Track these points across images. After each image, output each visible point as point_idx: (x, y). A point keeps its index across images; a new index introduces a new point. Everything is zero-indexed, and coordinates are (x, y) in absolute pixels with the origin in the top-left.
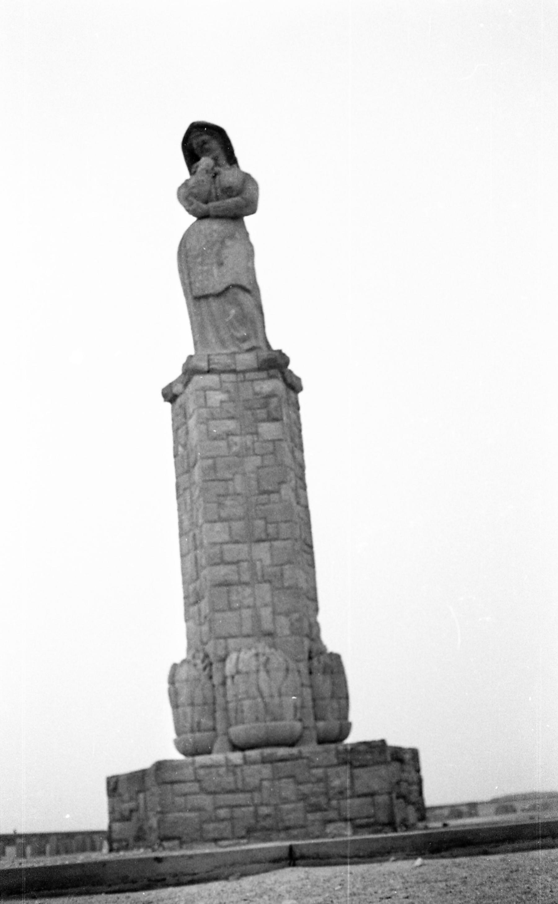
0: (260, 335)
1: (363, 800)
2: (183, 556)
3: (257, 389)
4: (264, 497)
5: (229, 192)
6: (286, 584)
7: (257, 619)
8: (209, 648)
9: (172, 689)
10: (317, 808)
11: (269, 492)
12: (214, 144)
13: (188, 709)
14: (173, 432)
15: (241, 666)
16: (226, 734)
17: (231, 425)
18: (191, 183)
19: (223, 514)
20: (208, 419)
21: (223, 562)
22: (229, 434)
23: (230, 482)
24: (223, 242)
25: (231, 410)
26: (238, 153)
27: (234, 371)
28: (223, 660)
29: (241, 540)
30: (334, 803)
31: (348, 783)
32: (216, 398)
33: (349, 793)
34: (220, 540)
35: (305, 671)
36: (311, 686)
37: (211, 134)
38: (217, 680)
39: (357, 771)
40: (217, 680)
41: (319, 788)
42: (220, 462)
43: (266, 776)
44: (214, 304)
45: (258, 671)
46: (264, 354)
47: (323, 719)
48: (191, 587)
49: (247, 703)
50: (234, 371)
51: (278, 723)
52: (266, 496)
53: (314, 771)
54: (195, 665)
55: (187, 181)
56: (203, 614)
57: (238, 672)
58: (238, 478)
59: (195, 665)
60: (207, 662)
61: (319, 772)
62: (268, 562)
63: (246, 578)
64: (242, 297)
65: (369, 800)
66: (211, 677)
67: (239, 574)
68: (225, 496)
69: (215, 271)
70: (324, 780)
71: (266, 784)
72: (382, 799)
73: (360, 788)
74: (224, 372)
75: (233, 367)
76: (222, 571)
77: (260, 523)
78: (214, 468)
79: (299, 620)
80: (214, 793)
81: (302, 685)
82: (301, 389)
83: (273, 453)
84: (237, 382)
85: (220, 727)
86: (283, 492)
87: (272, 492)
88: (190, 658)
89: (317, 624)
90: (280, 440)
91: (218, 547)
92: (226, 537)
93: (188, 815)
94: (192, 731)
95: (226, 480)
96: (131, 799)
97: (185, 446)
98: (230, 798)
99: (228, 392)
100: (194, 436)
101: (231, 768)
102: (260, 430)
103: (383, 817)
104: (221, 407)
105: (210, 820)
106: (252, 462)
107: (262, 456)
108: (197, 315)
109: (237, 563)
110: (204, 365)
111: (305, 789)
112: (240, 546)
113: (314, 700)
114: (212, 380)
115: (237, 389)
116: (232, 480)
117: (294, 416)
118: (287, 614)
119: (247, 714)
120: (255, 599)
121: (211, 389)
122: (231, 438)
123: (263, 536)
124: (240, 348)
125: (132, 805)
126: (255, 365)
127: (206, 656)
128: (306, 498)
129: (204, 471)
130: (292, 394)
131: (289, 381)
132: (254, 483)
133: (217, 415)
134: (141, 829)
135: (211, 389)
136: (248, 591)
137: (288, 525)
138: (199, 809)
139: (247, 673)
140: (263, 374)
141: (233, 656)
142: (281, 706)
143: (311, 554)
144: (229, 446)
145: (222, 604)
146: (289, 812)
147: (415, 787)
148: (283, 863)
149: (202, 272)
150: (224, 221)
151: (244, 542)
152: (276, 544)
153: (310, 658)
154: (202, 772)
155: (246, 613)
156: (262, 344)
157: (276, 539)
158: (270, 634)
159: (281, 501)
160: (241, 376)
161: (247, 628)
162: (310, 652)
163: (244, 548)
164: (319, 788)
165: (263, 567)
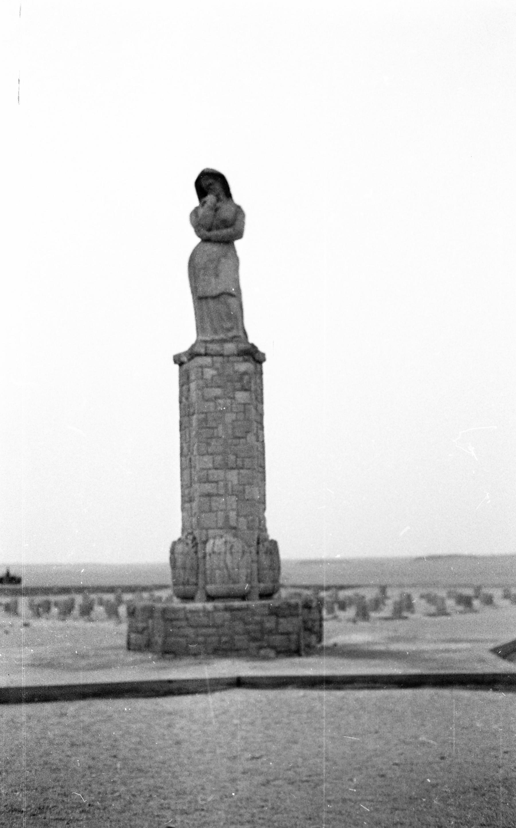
0: (240, 327)
3: (236, 368)
4: (235, 441)
6: (246, 498)
7: (227, 518)
8: (196, 533)
9: (172, 557)
10: (255, 640)
11: (239, 438)
12: (217, 187)
13: (182, 572)
14: (180, 386)
15: (216, 549)
16: (204, 588)
17: (218, 392)
18: (201, 211)
19: (210, 450)
20: (203, 388)
21: (208, 481)
22: (216, 398)
24: (219, 261)
26: (233, 190)
27: (222, 355)
28: (205, 542)
32: (209, 373)
36: (258, 562)
38: (200, 555)
39: (281, 620)
40: (200, 555)
41: (257, 628)
42: (210, 418)
44: (211, 303)
45: (225, 553)
46: (242, 346)
48: (187, 492)
49: (218, 572)
50: (222, 355)
54: (187, 544)
55: (197, 208)
56: (194, 511)
57: (214, 552)
58: (220, 428)
59: (187, 544)
60: (194, 542)
61: (257, 618)
62: (236, 482)
63: (222, 492)
65: (286, 636)
66: (196, 552)
67: (217, 488)
68: (211, 438)
69: (213, 280)
70: (261, 623)
72: (294, 637)
73: (281, 629)
74: (216, 355)
76: (208, 488)
77: (232, 457)
78: (205, 420)
79: (253, 521)
81: (252, 561)
82: (264, 360)
85: (201, 583)
86: (248, 439)
87: (242, 438)
88: (184, 537)
89: (264, 519)
90: (249, 404)
91: (206, 471)
93: (181, 640)
94: (184, 584)
95: (213, 428)
97: (187, 399)
98: (204, 630)
99: (217, 369)
100: (194, 396)
103: (293, 647)
104: (212, 379)
105: (193, 643)
106: (229, 417)
107: (237, 413)
108: (199, 309)
109: (217, 482)
110: (202, 351)
111: (250, 627)
112: (219, 471)
113: (258, 570)
114: (208, 360)
115: (223, 368)
117: (258, 381)
118: (245, 516)
119: (218, 580)
120: (227, 506)
121: (206, 367)
123: (234, 466)
125: (144, 625)
126: (236, 353)
127: (194, 539)
128: (263, 436)
129: (200, 421)
130: (258, 365)
132: (230, 432)
134: (149, 640)
135: (206, 367)
137: (250, 460)
138: (186, 636)
139: (219, 554)
140: (241, 359)
141: (211, 542)
142: (238, 575)
143: (264, 473)
144: (216, 407)
145: (206, 507)
146: (239, 640)
147: (317, 623)
151: (221, 469)
152: (242, 471)
153: (258, 543)
155: (221, 514)
156: (241, 334)
157: (242, 468)
158: (235, 528)
159: (247, 443)
160: (226, 359)
161: (220, 524)
162: (258, 539)
164: (257, 628)
165: (232, 486)
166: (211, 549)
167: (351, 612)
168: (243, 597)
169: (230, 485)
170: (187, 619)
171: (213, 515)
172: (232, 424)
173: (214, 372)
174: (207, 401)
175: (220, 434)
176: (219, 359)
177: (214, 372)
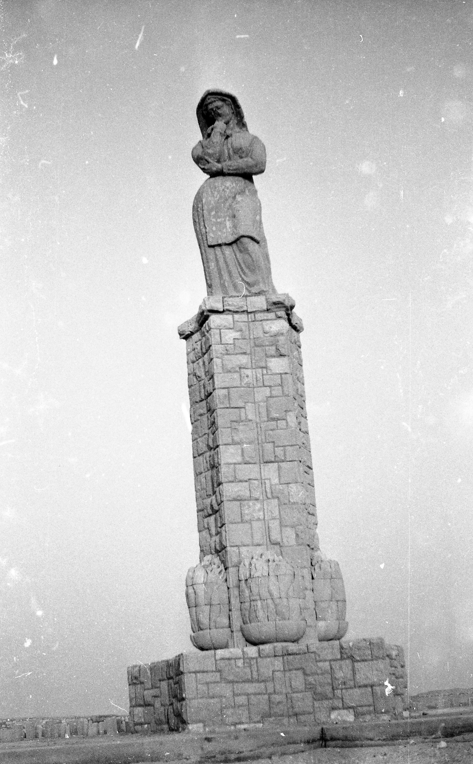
1: (363, 690)
2: (197, 474)
5: (239, 152)
12: (226, 110)
17: (244, 360)
23: (243, 410)
24: (234, 198)
25: (242, 346)
26: (247, 119)
29: (251, 461)
30: (338, 692)
31: (349, 675)
33: (352, 683)
34: (234, 461)
35: (308, 577)
37: (223, 100)
43: (277, 668)
47: (324, 619)
51: (286, 622)
52: (274, 423)
53: (320, 664)
58: (249, 406)
63: (257, 494)
64: (251, 245)
71: (278, 674)
74: (237, 312)
75: (245, 308)
80: (232, 682)
83: (281, 385)
84: (248, 322)
92: (239, 459)
96: (153, 687)
101: (248, 661)
102: (269, 364)
122: (242, 370)
124: (250, 292)
131: (294, 322)
132: (264, 414)
133: (231, 351)
136: (258, 506)
148: (317, 744)
149: (217, 223)
150: (236, 178)
152: (283, 465)
163: (256, 468)
165: (271, 485)
166: (215, 531)
168: (371, 740)
169: (268, 485)
171: (247, 526)
173: (237, 335)
175: (250, 417)
176: (244, 317)
177: (237, 335)
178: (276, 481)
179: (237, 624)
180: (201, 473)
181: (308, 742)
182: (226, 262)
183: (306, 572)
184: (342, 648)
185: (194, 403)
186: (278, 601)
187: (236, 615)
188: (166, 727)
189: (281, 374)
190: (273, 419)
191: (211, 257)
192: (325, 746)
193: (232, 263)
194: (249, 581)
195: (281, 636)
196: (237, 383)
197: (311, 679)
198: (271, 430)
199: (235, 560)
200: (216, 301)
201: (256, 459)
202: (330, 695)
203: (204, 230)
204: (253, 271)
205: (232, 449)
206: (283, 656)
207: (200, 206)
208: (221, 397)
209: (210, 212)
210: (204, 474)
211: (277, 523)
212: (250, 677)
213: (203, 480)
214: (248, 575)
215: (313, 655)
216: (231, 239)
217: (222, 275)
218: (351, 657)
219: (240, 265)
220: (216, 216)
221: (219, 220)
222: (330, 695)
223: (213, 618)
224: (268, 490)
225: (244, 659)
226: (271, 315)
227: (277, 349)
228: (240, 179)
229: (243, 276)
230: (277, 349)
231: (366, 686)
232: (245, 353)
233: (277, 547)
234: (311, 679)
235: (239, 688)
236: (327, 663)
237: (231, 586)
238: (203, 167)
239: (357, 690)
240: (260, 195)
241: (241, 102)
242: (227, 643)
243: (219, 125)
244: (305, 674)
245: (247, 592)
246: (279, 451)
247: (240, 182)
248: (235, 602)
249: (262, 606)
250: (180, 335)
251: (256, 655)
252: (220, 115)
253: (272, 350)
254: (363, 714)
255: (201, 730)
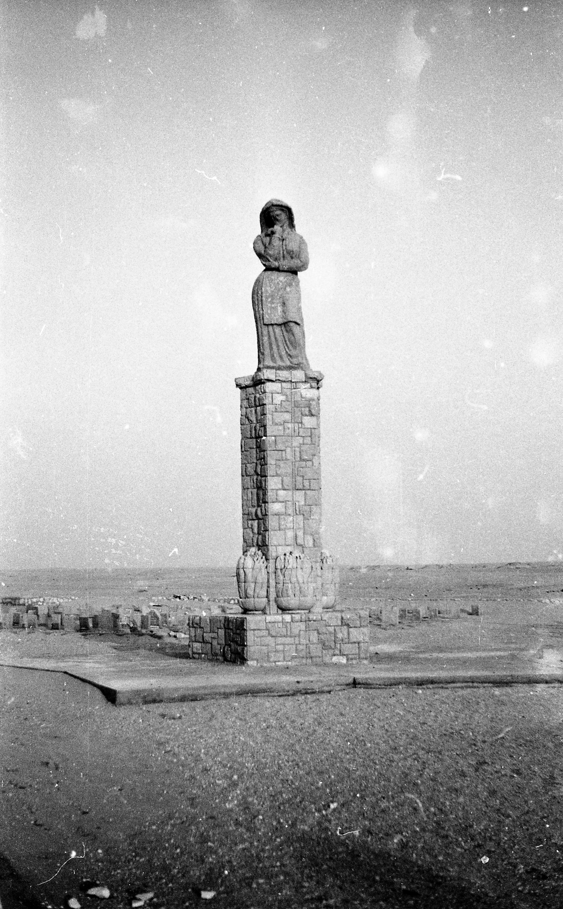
1: (354, 645)
2: (244, 489)
12: (283, 217)
17: (287, 416)
33: (347, 640)
35: (319, 568)
37: (282, 210)
43: (302, 629)
61: (331, 629)
116: (285, 450)
132: (298, 454)
138: (267, 645)
148: (350, 686)
149: (271, 308)
154: (270, 625)
163: (290, 493)
167: (19, 786)
170: (267, 629)
172: (300, 447)
173: (283, 398)
174: (276, 424)
175: (289, 457)
177: (283, 398)
178: (303, 503)
179: (273, 596)
180: (248, 489)
181: (347, 685)
182: (276, 338)
183: (318, 565)
184: (342, 618)
185: (244, 437)
186: (302, 585)
187: (272, 590)
188: (221, 658)
189: (311, 428)
190: (304, 460)
191: (265, 333)
192: (355, 687)
193: (280, 338)
194: (284, 570)
195: (301, 607)
196: (282, 433)
197: (322, 637)
198: (302, 468)
199: (274, 554)
200: (272, 374)
201: (290, 488)
202: (333, 647)
203: (261, 312)
204: (295, 348)
205: (276, 479)
206: (306, 621)
207: (260, 292)
208: (271, 442)
209: (267, 298)
210: (250, 490)
211: (302, 531)
212: (285, 634)
213: (250, 495)
214: (283, 566)
215: (324, 622)
216: (281, 321)
217: (272, 348)
218: (348, 625)
219: (286, 341)
220: (272, 303)
221: (273, 306)
222: (333, 647)
223: (257, 591)
224: (298, 510)
225: (282, 622)
226: (308, 385)
227: (310, 411)
228: (290, 274)
229: (287, 350)
230: (310, 411)
231: (355, 643)
232: (288, 412)
233: (301, 548)
234: (322, 637)
235: (280, 640)
236: (333, 628)
237: (270, 571)
238: (264, 263)
239: (350, 645)
240: (301, 285)
241: (294, 211)
242: (265, 607)
243: (277, 228)
244: (319, 633)
245: (281, 577)
246: (306, 483)
247: (290, 276)
248: (272, 582)
249: (291, 587)
250: (237, 385)
251: (290, 621)
252: (277, 220)
253: (306, 411)
254: (352, 659)
255: (255, 665)
